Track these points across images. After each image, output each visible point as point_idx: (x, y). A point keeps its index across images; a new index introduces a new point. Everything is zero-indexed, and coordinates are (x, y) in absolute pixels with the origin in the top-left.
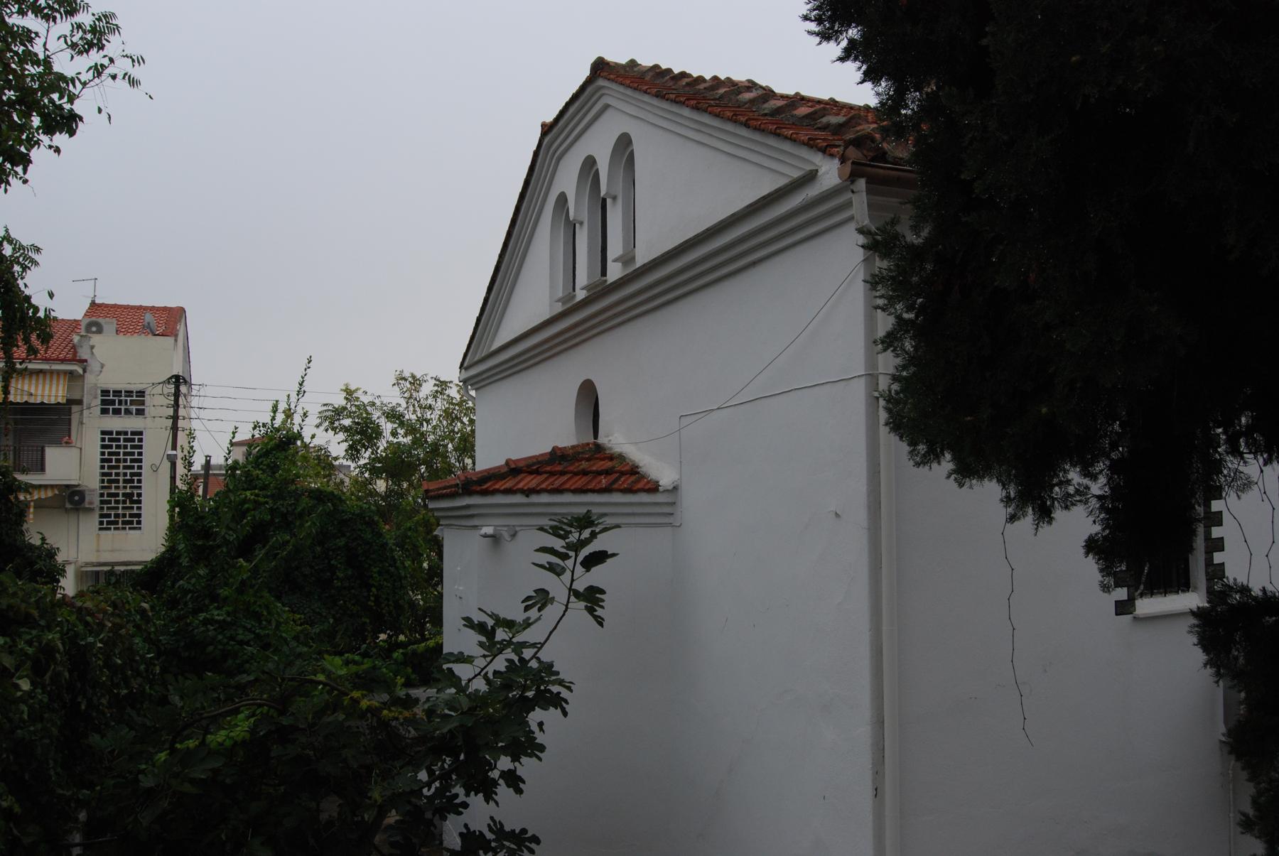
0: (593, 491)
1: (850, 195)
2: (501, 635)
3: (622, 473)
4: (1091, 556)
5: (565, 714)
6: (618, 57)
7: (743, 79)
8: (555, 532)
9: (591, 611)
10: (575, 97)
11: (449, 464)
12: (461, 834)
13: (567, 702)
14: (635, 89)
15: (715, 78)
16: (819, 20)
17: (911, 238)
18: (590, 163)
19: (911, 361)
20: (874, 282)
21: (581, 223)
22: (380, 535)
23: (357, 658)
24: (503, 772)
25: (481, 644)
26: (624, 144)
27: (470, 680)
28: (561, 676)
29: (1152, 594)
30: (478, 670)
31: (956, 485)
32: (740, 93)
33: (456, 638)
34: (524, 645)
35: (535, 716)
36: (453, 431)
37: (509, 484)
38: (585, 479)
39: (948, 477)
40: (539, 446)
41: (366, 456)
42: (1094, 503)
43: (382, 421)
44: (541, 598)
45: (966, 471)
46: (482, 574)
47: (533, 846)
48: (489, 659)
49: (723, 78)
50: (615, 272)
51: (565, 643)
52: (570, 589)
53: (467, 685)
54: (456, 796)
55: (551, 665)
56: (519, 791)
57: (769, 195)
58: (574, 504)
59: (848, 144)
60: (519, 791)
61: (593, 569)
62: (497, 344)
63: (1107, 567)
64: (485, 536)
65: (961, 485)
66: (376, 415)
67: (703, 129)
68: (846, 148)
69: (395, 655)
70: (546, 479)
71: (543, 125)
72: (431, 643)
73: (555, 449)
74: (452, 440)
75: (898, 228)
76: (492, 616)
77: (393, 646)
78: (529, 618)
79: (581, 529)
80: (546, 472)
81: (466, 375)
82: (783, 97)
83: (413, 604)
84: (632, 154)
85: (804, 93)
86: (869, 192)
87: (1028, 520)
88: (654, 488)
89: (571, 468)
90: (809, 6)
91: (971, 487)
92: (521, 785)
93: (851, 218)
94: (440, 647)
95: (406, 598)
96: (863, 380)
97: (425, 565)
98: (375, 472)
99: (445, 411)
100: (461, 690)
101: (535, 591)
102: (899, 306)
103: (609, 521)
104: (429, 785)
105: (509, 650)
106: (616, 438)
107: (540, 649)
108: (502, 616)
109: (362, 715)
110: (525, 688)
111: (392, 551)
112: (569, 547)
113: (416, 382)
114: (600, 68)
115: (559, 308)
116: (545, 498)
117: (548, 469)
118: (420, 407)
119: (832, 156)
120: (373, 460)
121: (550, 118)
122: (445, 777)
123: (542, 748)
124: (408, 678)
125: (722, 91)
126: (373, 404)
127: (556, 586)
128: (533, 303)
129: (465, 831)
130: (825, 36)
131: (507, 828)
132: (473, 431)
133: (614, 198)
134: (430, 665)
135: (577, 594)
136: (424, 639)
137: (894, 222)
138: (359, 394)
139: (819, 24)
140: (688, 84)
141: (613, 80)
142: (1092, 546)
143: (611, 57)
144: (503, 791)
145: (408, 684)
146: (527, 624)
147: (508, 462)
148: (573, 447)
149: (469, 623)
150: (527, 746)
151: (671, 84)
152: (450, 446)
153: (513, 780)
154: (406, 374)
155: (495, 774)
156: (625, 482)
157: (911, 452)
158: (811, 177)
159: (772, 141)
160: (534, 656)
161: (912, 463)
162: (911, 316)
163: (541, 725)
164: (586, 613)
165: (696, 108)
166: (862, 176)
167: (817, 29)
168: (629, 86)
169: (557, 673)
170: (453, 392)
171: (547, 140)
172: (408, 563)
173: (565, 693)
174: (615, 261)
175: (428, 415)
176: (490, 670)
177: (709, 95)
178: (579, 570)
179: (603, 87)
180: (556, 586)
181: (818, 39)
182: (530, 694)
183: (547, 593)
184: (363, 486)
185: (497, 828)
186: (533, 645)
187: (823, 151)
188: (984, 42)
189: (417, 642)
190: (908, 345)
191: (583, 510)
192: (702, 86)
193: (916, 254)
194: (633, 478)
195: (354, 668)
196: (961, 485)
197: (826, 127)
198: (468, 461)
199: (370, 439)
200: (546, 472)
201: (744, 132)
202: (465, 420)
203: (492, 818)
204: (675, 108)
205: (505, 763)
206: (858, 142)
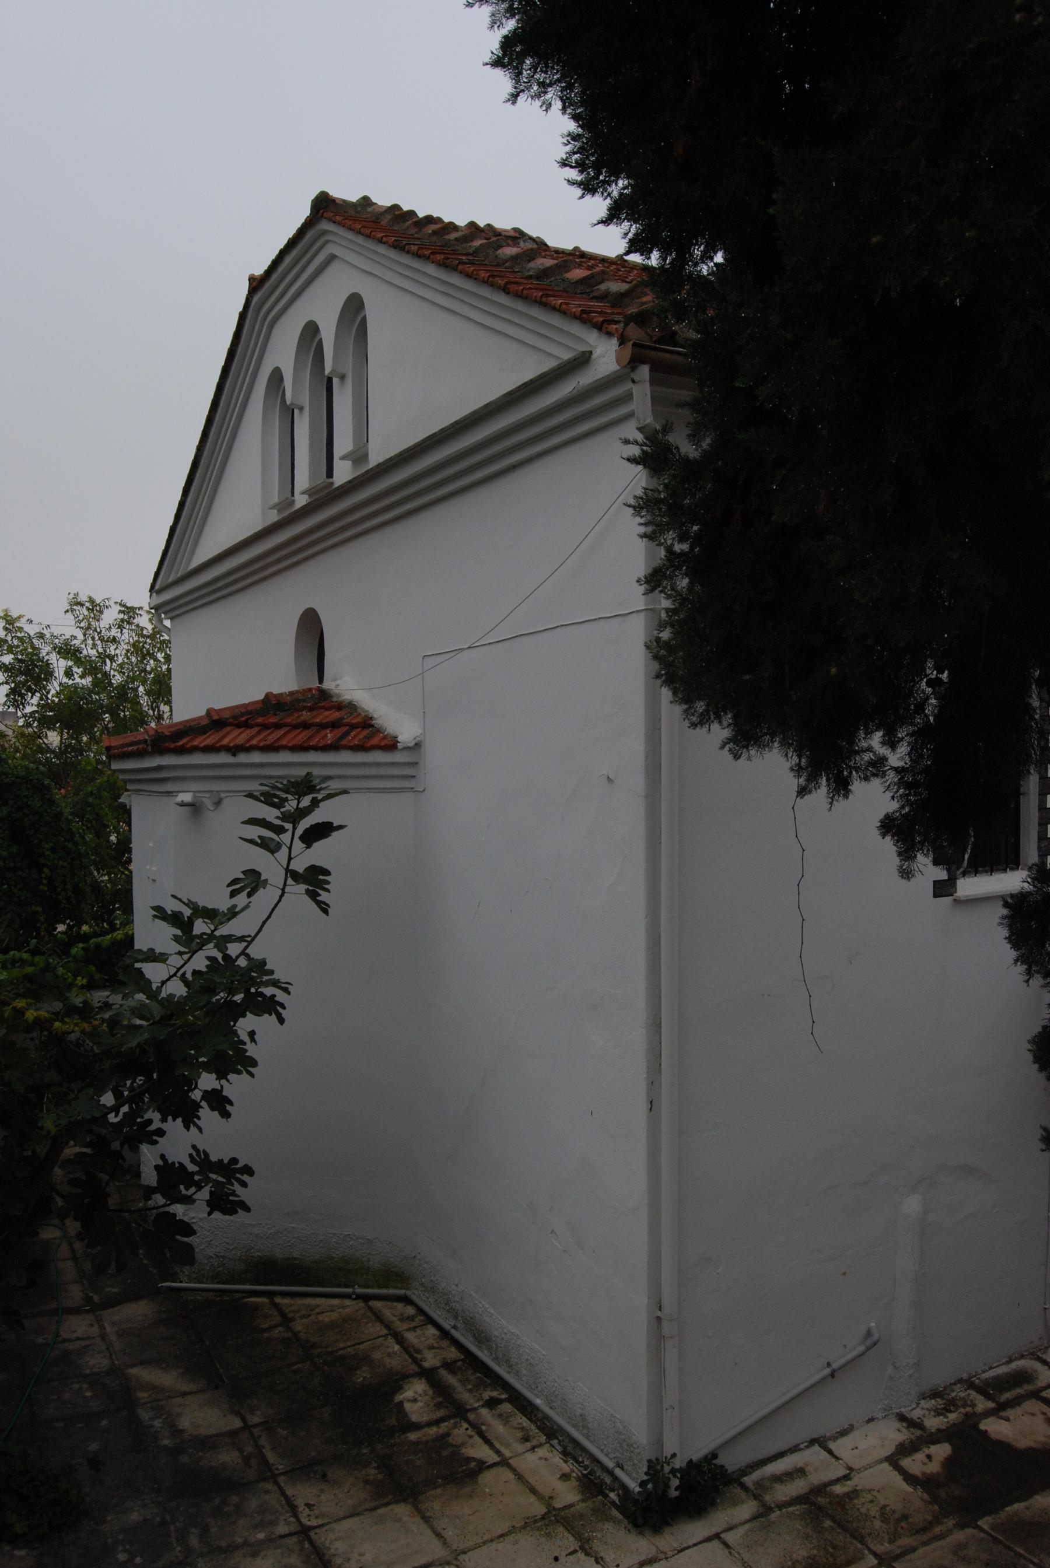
0: (316, 748)
1: (630, 385)
2: (200, 927)
3: (353, 727)
4: (888, 838)
5: (281, 1020)
6: (347, 192)
7: (508, 227)
8: (268, 799)
9: (313, 895)
10: (292, 244)
11: (141, 713)
12: (157, 1167)
13: (283, 1006)
14: (368, 236)
15: (472, 225)
16: (581, 166)
17: (689, 450)
18: (311, 330)
19: (682, 600)
20: (644, 504)
21: (301, 409)
22: (52, 802)
23: (25, 956)
24: (206, 1092)
25: (176, 939)
26: (354, 306)
27: (164, 983)
28: (275, 976)
29: (976, 873)
30: (173, 971)
31: (730, 757)
32: (501, 247)
33: (150, 933)
34: (229, 938)
35: (245, 1024)
36: (145, 670)
37: (210, 740)
38: (306, 734)
39: (722, 747)
40: (249, 692)
41: (32, 704)
42: (892, 777)
43: (53, 658)
44: (251, 882)
45: (745, 738)
46: (177, 852)
47: (245, 1178)
48: (186, 957)
49: (482, 225)
50: (343, 473)
51: (281, 936)
52: (287, 870)
53: (159, 989)
54: (150, 1122)
55: (264, 963)
56: (226, 1115)
57: (532, 381)
58: (290, 764)
59: (630, 319)
60: (226, 1115)
61: (315, 845)
62: (195, 563)
63: (906, 851)
64: (182, 804)
65: (737, 757)
66: (45, 650)
67: (452, 292)
68: (626, 324)
69: (74, 951)
70: (258, 733)
71: (252, 279)
72: (119, 935)
73: (268, 696)
74: (144, 682)
75: (671, 438)
76: (190, 904)
77: (74, 937)
78: (235, 906)
79: (300, 796)
80: (257, 725)
81: (158, 600)
82: (557, 251)
83: (97, 887)
84: (320, 341)
85: (585, 248)
86: (653, 382)
87: (821, 793)
88: (391, 745)
89: (289, 720)
90: (568, 148)
91: (749, 759)
92: (229, 1108)
93: (630, 415)
94: (130, 940)
95: (89, 880)
96: (642, 617)
97: (113, 838)
98: (46, 723)
99: (134, 645)
100: (153, 995)
101: (244, 872)
102: (670, 536)
103: (335, 785)
104: (116, 1109)
105: (211, 945)
106: (346, 682)
107: (250, 943)
108: (201, 904)
109: (29, 1028)
110: (231, 992)
111: (69, 822)
112: (285, 817)
113: (96, 609)
114: (324, 206)
115: (274, 517)
116: (256, 757)
117: (260, 720)
118: (102, 640)
119: (609, 334)
120: (44, 706)
121: (259, 271)
122: (135, 1099)
123: (254, 1063)
124: (91, 978)
125: (477, 243)
126: (41, 636)
127: (271, 867)
128: (242, 509)
129: (161, 1163)
130: (589, 187)
131: (214, 1158)
132: (169, 670)
133: (343, 377)
134: (117, 963)
135: (295, 876)
136: (113, 928)
137: (667, 428)
138: (22, 623)
139: (581, 172)
140: (435, 233)
141: (339, 224)
142: (888, 825)
143: (336, 193)
144: (207, 1115)
145: (92, 986)
146: (233, 913)
147: (209, 712)
148: (291, 693)
149: (160, 913)
150: (234, 1060)
151: (413, 231)
152: (141, 689)
153: (219, 1102)
154: (83, 598)
155: (196, 1095)
156: (356, 737)
157: (686, 711)
158: (583, 360)
159: (536, 312)
160: (243, 953)
161: (687, 723)
162: (685, 547)
163: (252, 1034)
164: (306, 897)
165: (443, 265)
166: (644, 362)
167: (579, 179)
168: (359, 233)
169: (272, 972)
170: (144, 621)
171: (255, 299)
172: (89, 837)
173: (281, 996)
174: (344, 458)
175: (112, 650)
176: (188, 969)
177: (459, 247)
178: (298, 845)
179: (325, 232)
180: (271, 867)
181: (579, 192)
182: (238, 998)
183: (259, 874)
184: (31, 740)
185: (201, 1158)
186: (242, 939)
187: (599, 327)
188: (771, 211)
189: (104, 933)
190: (683, 583)
191: (301, 772)
192: (453, 236)
193: (690, 470)
194: (365, 732)
195: (16, 972)
196: (737, 757)
197: (604, 296)
198: (164, 708)
199: (38, 681)
200: (257, 725)
201: (502, 299)
202: (160, 656)
203: (194, 1147)
204: (417, 264)
205: (207, 1081)
206: (641, 319)
